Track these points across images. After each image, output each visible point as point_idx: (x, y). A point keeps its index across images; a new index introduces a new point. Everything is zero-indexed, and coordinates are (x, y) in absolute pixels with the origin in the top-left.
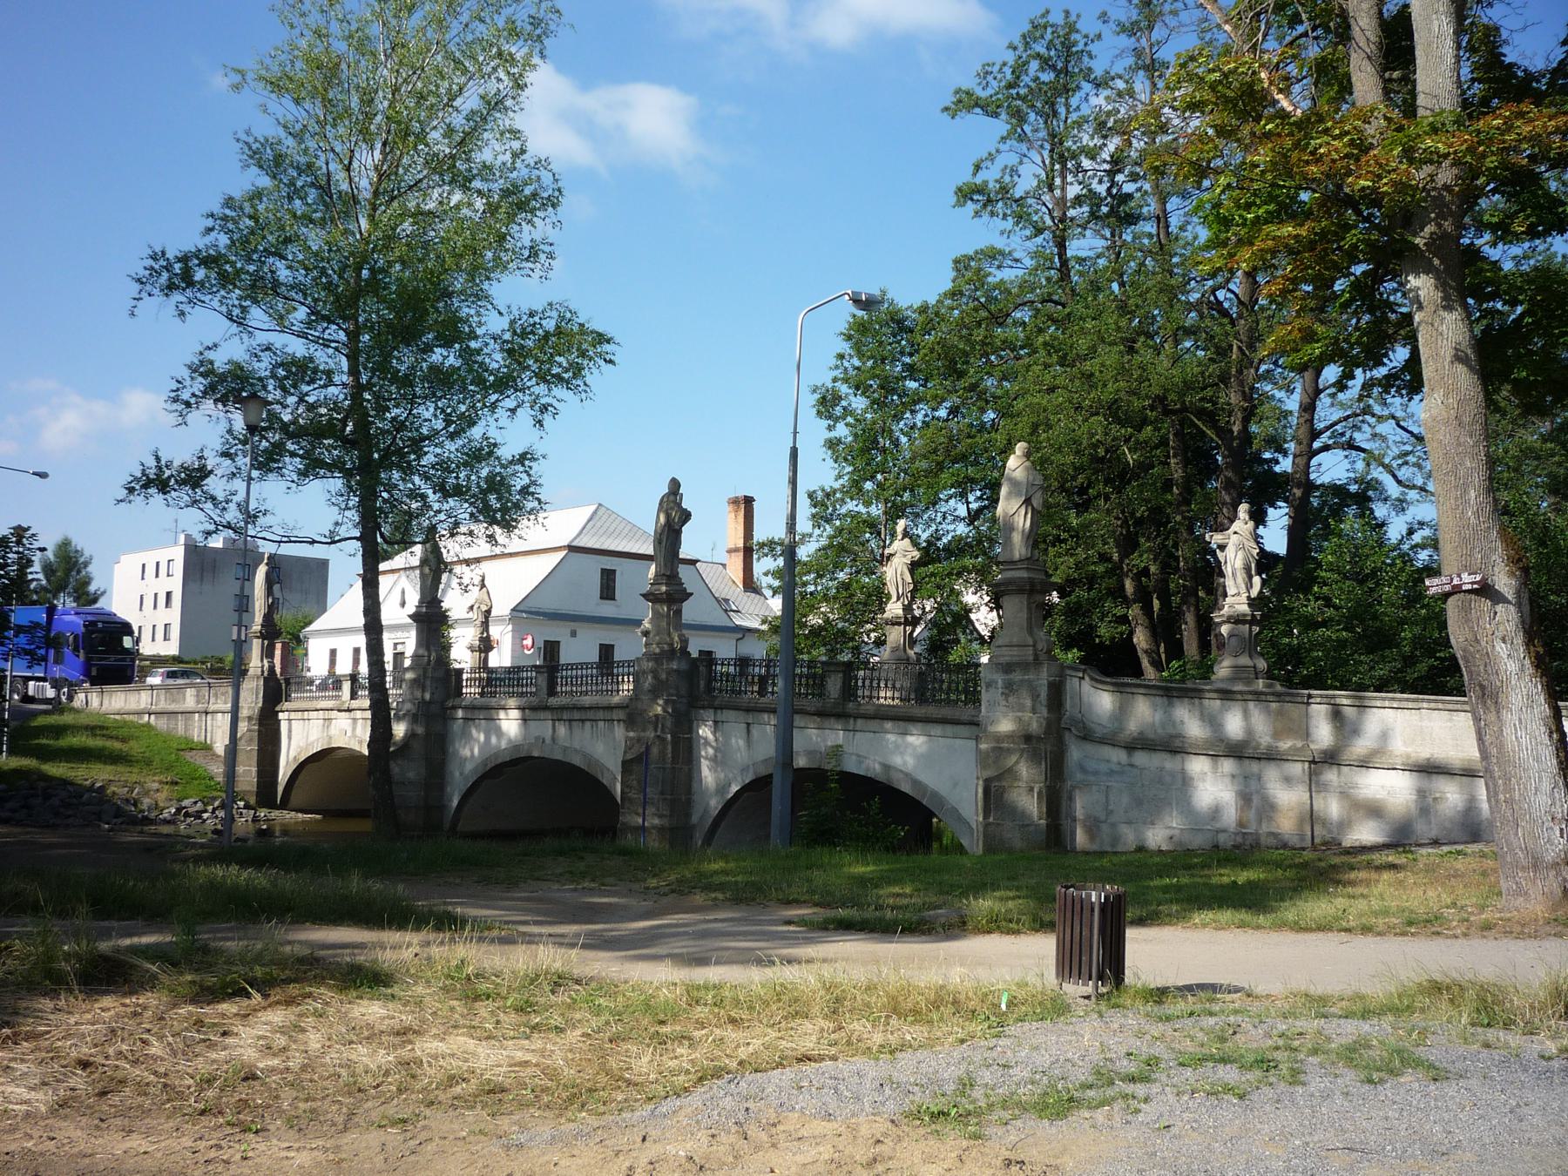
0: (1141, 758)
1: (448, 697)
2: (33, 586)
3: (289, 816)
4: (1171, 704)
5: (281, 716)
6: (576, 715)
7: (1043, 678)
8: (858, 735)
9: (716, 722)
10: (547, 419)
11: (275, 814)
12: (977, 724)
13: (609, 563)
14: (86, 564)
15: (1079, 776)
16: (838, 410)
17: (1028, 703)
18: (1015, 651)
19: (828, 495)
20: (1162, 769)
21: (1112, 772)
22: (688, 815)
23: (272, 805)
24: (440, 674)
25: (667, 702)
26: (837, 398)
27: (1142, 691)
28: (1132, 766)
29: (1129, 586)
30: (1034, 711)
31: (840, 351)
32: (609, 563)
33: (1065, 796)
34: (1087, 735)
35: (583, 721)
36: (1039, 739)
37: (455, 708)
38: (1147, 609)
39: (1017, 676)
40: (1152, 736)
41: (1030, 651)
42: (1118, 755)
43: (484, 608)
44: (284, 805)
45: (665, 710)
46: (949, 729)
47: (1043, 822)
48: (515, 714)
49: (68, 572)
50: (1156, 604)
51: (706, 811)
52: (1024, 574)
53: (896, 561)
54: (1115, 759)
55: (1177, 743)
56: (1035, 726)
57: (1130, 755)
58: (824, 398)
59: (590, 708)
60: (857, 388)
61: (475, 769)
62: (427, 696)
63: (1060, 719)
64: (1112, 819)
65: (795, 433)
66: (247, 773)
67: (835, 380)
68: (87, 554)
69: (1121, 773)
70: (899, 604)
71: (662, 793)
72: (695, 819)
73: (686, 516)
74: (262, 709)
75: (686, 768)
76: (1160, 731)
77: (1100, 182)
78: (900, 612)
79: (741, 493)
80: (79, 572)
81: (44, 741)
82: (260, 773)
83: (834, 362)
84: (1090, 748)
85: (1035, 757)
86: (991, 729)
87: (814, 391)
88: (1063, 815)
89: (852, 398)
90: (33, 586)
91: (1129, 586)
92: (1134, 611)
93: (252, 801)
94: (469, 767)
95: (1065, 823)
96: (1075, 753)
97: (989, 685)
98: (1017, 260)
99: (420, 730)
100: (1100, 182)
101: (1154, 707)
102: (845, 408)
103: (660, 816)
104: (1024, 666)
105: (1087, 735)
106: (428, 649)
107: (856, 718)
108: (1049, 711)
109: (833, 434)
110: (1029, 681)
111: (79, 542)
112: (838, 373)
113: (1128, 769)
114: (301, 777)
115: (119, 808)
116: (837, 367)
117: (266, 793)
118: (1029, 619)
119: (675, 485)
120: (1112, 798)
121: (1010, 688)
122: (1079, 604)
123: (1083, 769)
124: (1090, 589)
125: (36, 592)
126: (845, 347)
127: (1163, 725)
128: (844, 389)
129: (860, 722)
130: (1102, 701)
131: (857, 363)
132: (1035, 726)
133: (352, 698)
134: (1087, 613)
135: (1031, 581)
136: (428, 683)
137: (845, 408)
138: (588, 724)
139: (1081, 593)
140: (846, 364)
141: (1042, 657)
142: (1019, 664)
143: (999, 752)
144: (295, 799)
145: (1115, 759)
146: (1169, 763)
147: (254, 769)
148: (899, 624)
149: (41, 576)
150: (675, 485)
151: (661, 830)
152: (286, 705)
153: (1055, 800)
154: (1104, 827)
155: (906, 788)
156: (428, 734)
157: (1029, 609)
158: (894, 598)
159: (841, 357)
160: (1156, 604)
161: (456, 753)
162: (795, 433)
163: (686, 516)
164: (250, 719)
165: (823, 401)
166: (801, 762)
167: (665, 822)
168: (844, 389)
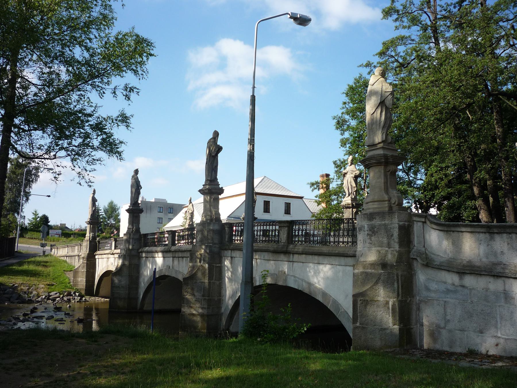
0: (469, 281)
1: (140, 248)
2: (101, 217)
3: (98, 299)
4: (492, 239)
5: (96, 257)
6: (180, 255)
7: (395, 223)
8: (295, 264)
9: (232, 257)
10: (133, 96)
11: (93, 298)
12: (354, 256)
13: (267, 198)
14: (118, 209)
15: (424, 293)
16: (345, 127)
17: (385, 240)
18: (376, 205)
19: (342, 163)
20: (487, 290)
21: (448, 291)
22: (220, 308)
23: (92, 295)
24: (137, 236)
25: (206, 247)
26: (345, 121)
27: (469, 229)
28: (463, 286)
29: (476, 190)
30: (389, 246)
31: (345, 101)
32: (267, 198)
33: (414, 307)
34: (429, 263)
35: (183, 257)
36: (392, 266)
37: (142, 252)
38: (486, 201)
39: (377, 222)
40: (478, 264)
41: (386, 204)
42: (452, 278)
43: (190, 212)
44: (97, 295)
45: (205, 251)
46: (343, 260)
47: (396, 327)
48: (160, 255)
49: (112, 212)
50: (491, 199)
51: (227, 306)
52: (381, 152)
53: (348, 176)
54: (450, 281)
55: (499, 269)
56: (391, 258)
57: (461, 279)
58: (338, 121)
59: (185, 251)
60: (353, 116)
61: (148, 280)
62: (131, 247)
63: (409, 252)
64: (450, 326)
65: (254, 87)
66: (82, 281)
67: (342, 114)
68: (118, 206)
69: (455, 292)
70: (350, 198)
71: (203, 296)
72: (223, 310)
73: (220, 149)
74: (88, 254)
75: (218, 282)
76: (484, 260)
77: (455, 7)
78: (350, 202)
79: (324, 173)
80: (116, 212)
81: (14, 267)
82: (87, 281)
83: (341, 105)
84: (431, 272)
85: (388, 283)
86: (362, 259)
87: (334, 119)
88: (414, 321)
89: (351, 121)
90: (101, 217)
91: (476, 190)
92: (479, 203)
93: (83, 292)
94: (146, 279)
95: (415, 328)
96: (422, 277)
97: (360, 229)
98: (413, 40)
99: (127, 263)
100: (455, 7)
101: (479, 242)
102: (348, 126)
103: (202, 308)
104: (382, 215)
105: (429, 263)
106: (133, 226)
107: (293, 254)
108: (401, 245)
109: (344, 136)
110: (385, 225)
111: (116, 202)
112: (344, 110)
113: (459, 288)
114: (103, 282)
115: (20, 295)
116: (343, 108)
117: (90, 290)
118: (386, 183)
119: (216, 134)
120: (449, 311)
121: (373, 231)
122: (454, 204)
123: (427, 289)
124: (459, 197)
125: (102, 219)
126: (347, 99)
127: (487, 256)
128: (347, 117)
129: (296, 256)
130: (436, 240)
131: (351, 105)
132: (391, 258)
133: (115, 249)
134: (459, 208)
135: (385, 156)
136: (131, 241)
137: (348, 126)
138: (184, 259)
139: (455, 199)
140: (347, 106)
141: (395, 208)
142: (378, 214)
143: (366, 277)
144: (102, 292)
145: (450, 281)
146: (495, 285)
147: (85, 279)
148: (349, 208)
149: (103, 213)
150: (216, 134)
151: (202, 315)
152: (98, 252)
153: (405, 313)
154: (444, 332)
155: (320, 298)
156: (130, 264)
157: (386, 176)
158: (347, 195)
159: (345, 103)
160: (491, 199)
161: (143, 273)
162: (254, 87)
163: (220, 149)
164: (83, 258)
165: (338, 123)
166: (258, 282)
167: (205, 312)
168: (347, 117)
